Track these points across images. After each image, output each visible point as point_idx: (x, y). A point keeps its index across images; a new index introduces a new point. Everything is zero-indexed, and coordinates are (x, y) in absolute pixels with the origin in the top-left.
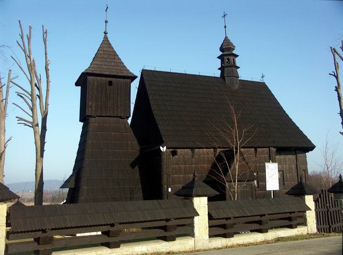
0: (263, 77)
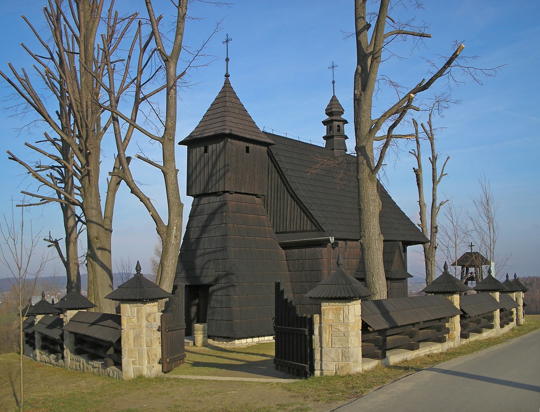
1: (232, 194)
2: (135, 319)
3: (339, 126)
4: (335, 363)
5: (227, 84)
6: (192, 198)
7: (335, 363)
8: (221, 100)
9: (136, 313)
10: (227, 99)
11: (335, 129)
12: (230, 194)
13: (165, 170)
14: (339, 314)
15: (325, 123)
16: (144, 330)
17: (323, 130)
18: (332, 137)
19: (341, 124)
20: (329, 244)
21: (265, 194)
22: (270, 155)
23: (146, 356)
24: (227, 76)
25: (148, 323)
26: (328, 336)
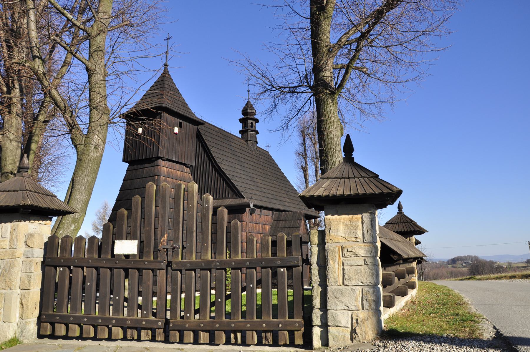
0: (268, 146)
1: (164, 160)
2: (8, 243)
3: (252, 123)
4: (350, 313)
5: (166, 71)
6: (127, 165)
7: (350, 313)
8: (160, 83)
9: (9, 232)
10: (165, 82)
11: (250, 125)
12: (163, 160)
13: (89, 65)
14: (356, 228)
15: (241, 121)
16: (20, 261)
17: (240, 126)
18: (247, 131)
19: (254, 122)
20: (248, 210)
21: (193, 165)
22: (199, 136)
23: (18, 304)
24: (166, 65)
25: (28, 249)
26: (337, 266)
